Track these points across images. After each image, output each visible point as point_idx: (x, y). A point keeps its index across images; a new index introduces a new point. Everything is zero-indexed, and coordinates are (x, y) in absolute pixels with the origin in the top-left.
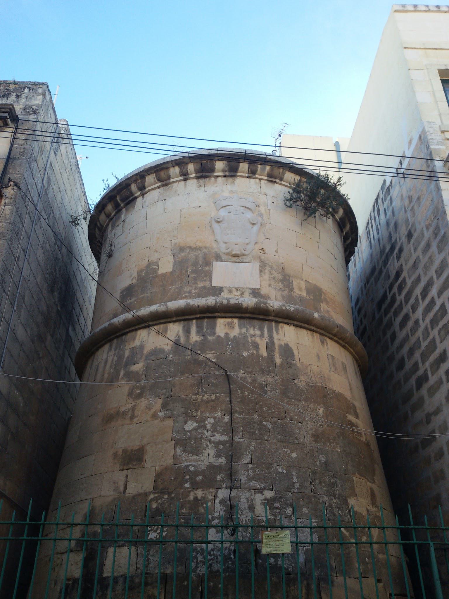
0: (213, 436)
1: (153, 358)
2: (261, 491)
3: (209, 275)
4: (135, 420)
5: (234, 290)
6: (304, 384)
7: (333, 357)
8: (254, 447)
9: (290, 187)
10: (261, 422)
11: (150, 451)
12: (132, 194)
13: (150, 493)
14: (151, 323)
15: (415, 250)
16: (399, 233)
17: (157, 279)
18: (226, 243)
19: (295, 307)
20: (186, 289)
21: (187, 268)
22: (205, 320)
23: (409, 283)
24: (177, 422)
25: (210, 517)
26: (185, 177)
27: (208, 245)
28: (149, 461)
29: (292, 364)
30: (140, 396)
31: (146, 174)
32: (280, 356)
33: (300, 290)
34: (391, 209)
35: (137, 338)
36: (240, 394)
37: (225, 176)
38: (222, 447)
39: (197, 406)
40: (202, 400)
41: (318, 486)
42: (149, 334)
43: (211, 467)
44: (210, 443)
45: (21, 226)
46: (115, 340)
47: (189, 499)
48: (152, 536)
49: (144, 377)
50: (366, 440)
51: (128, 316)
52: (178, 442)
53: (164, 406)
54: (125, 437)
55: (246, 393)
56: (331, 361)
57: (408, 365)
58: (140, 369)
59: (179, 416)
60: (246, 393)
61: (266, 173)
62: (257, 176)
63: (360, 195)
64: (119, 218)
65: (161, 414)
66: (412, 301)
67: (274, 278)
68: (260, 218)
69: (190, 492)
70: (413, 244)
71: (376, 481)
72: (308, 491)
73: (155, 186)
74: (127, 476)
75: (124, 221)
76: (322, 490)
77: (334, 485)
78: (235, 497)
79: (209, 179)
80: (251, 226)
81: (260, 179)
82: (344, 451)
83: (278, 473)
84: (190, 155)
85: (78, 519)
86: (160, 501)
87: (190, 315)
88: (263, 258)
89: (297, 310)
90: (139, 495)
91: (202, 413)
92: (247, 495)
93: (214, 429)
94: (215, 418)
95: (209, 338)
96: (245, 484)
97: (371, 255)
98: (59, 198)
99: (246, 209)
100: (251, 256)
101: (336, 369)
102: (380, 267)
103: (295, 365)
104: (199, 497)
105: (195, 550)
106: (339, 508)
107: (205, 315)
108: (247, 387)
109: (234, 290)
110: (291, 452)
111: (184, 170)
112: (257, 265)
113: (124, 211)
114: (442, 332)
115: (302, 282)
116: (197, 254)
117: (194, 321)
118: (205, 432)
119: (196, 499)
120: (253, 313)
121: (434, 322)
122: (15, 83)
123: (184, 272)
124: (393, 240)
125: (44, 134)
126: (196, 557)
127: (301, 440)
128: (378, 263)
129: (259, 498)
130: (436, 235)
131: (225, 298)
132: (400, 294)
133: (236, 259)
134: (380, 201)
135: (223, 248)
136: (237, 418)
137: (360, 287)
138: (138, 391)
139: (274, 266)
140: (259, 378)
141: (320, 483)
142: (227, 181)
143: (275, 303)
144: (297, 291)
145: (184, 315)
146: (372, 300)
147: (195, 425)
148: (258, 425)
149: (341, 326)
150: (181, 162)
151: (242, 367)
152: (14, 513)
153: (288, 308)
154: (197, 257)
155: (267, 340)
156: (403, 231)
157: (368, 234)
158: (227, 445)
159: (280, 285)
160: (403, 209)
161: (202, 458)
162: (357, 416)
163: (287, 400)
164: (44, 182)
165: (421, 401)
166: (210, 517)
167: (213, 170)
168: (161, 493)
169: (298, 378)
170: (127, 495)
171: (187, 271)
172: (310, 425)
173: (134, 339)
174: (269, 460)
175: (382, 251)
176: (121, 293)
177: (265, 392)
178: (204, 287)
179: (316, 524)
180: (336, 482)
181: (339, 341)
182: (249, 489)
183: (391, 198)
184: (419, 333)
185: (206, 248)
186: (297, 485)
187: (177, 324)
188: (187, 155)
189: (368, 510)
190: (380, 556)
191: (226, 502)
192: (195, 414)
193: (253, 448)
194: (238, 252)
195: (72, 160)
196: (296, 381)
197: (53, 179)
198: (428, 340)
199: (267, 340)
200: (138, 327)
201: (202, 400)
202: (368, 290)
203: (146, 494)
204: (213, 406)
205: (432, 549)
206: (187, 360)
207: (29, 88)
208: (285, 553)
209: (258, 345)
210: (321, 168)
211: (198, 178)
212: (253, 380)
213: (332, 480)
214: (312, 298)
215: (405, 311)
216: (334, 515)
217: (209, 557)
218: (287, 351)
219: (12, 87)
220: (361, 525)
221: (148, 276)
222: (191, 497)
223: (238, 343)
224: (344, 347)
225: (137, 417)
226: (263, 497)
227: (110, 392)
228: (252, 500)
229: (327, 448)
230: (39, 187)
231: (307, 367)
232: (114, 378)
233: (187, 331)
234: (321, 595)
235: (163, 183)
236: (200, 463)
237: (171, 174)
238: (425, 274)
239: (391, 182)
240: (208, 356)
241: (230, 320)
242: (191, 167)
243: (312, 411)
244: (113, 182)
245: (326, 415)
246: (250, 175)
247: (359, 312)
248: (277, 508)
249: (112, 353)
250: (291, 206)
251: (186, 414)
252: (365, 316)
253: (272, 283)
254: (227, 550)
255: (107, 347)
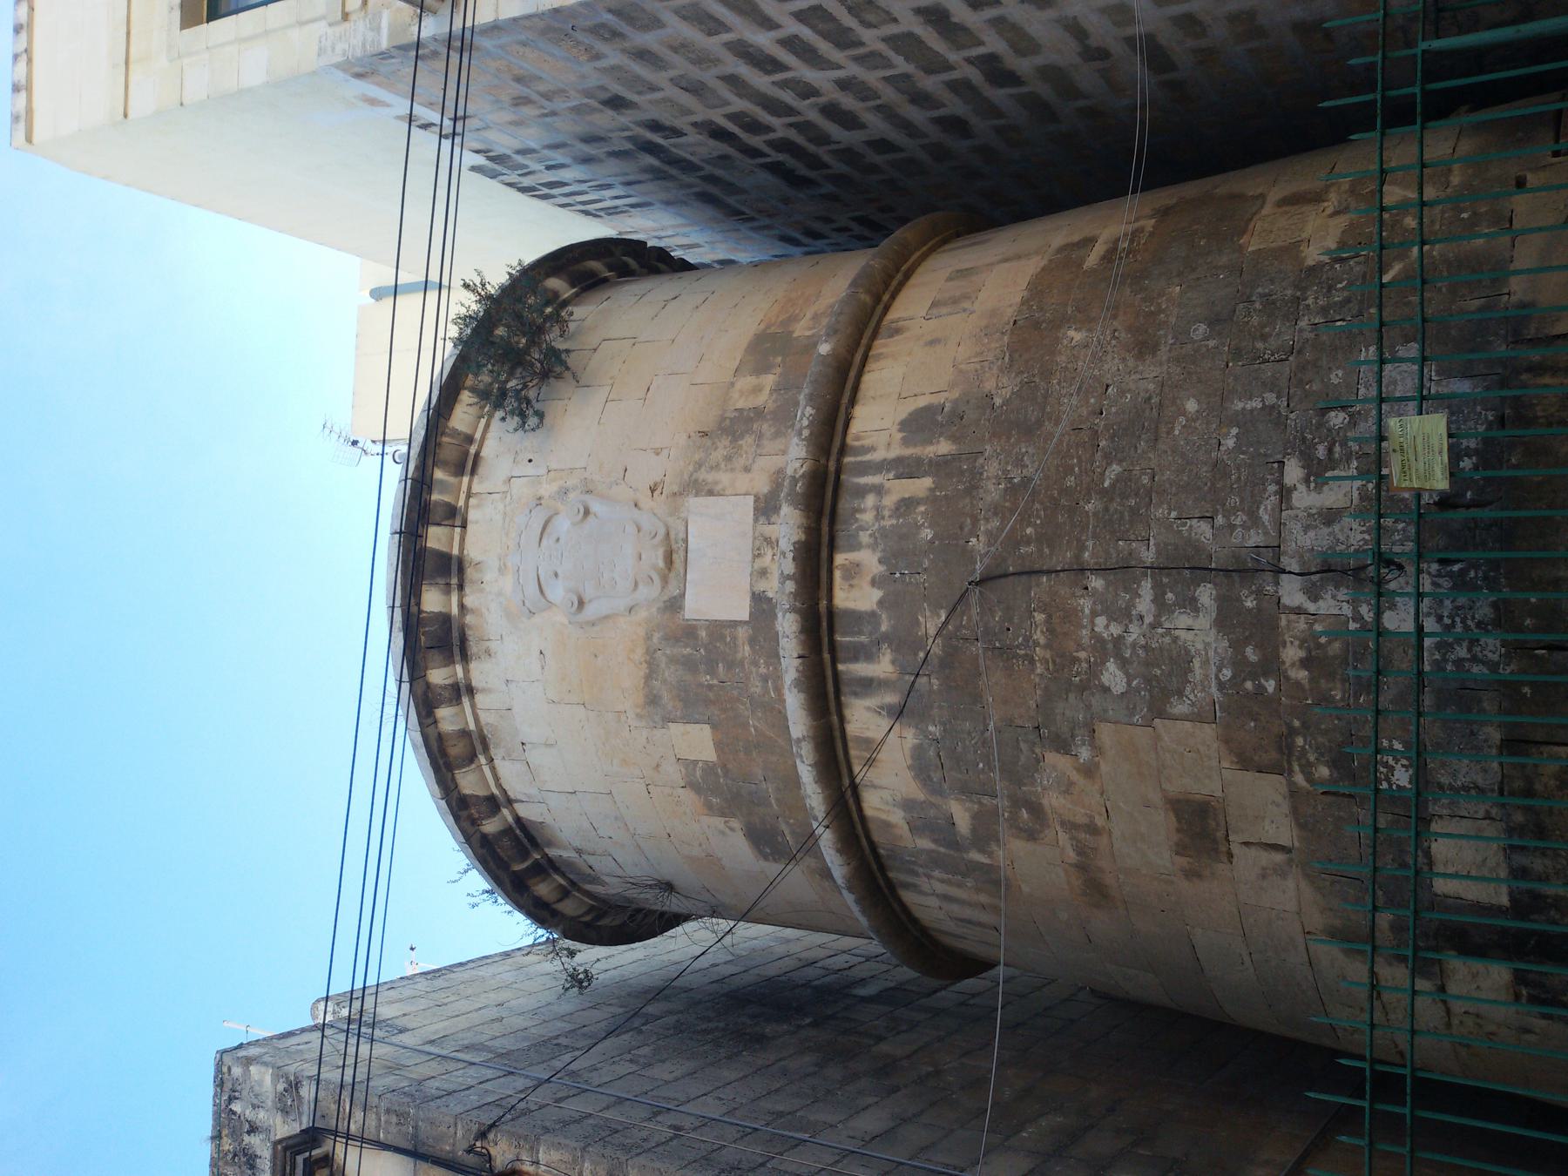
0: (1142, 617)
1: (936, 776)
2: (1285, 493)
3: (720, 629)
4: (1100, 821)
5: (759, 564)
6: (1005, 380)
7: (934, 305)
8: (1170, 510)
9: (491, 416)
10: (1104, 493)
11: (1179, 785)
12: (507, 831)
13: (1291, 784)
14: (846, 782)
15: (653, 88)
16: (611, 131)
17: (730, 766)
18: (636, 584)
19: (802, 402)
20: (758, 690)
21: (701, 685)
22: (838, 638)
23: (739, 104)
24: (1105, 711)
25: (1353, 626)
26: (461, 691)
27: (641, 632)
28: (1208, 787)
29: (953, 412)
30: (1037, 810)
31: (455, 794)
32: (932, 443)
33: (760, 390)
34: (546, 152)
35: (884, 816)
36: (1032, 548)
37: (461, 587)
38: (1170, 595)
39: (1063, 660)
40: (1047, 646)
41: (1273, 343)
42: (875, 787)
43: (1221, 623)
44: (1160, 625)
45: (591, 1121)
46: (891, 875)
47: (1305, 682)
48: (1402, 777)
49: (986, 800)
50: (1152, 217)
51: (827, 841)
52: (1159, 711)
53: (1063, 745)
54: (1144, 849)
55: (1029, 531)
56: (944, 310)
57: (955, 106)
58: (967, 810)
59: (1089, 707)
60: (1029, 531)
61: (452, 480)
62: (461, 503)
63: (509, 233)
64: (570, 864)
65: (1085, 754)
66: (788, 97)
67: (728, 459)
68: (572, 496)
69: (1287, 678)
70: (639, 93)
71: (1259, 191)
72: (1286, 369)
73: (486, 770)
74: (1246, 844)
75: (579, 851)
76: (1282, 334)
77: (1269, 302)
78: (1302, 562)
79: (470, 628)
80: (591, 518)
81: (469, 495)
82: (1180, 274)
83: (1238, 448)
84: (406, 677)
85: (1358, 971)
86: (1312, 758)
87: (824, 677)
88: (675, 488)
89: (811, 399)
90: (1295, 811)
91: (1080, 647)
92: (1295, 528)
93: (1125, 615)
94: (1094, 614)
95: (884, 628)
96: (1266, 533)
97: (668, 203)
98: (520, 1022)
99: (548, 530)
100: (670, 520)
101: (966, 297)
102: (698, 181)
103: (956, 402)
104: (1302, 654)
105: (1439, 666)
106: (1329, 290)
107: (826, 640)
108: (1013, 529)
109: (759, 564)
110: (1184, 413)
111: (446, 694)
112: (694, 503)
113: (553, 852)
114: (870, 17)
115: (738, 386)
116: (664, 659)
117: (841, 667)
118: (1130, 639)
119: (1305, 663)
120: (819, 514)
121: (843, 39)
122: (217, 1137)
123: (711, 695)
124: (628, 146)
125: (350, 1061)
126: (1459, 663)
127: (1151, 386)
128: (690, 186)
129: (1304, 499)
130: (616, 35)
131: (780, 584)
132: (769, 129)
133: (678, 559)
134: (527, 182)
135: (650, 592)
136: (1093, 555)
137: (751, 234)
138: (1024, 814)
139: (697, 457)
140: (989, 499)
141: (1264, 338)
142: (472, 582)
143: (794, 456)
144: (762, 399)
145: (826, 693)
146: (786, 201)
147: (1111, 666)
148: (1112, 500)
149: (854, 284)
150: (425, 702)
151: (962, 542)
152: (1343, 1138)
153: (805, 422)
154: (673, 660)
155: (891, 476)
156: (606, 120)
157: (612, 212)
158: (1165, 580)
159: (748, 441)
160: (548, 119)
161: (1200, 646)
162: (1090, 242)
163: (1048, 426)
164: (476, 1060)
165: (1050, 73)
166: (1353, 626)
167: (445, 619)
168: (1290, 755)
169: (990, 396)
170: (1297, 844)
171: (710, 687)
172: (1112, 365)
173: (887, 825)
174: (1204, 471)
175: (658, 175)
176: (766, 858)
177: (1026, 481)
178: (752, 641)
179: (1372, 349)
180: (1261, 296)
181: (892, 288)
182: (1280, 525)
183: (518, 152)
184: (872, 78)
185: (649, 637)
186: (1271, 398)
187: (847, 713)
188: (406, 687)
189: (1336, 213)
190: (1456, 180)
191: (1314, 584)
192: (1085, 665)
193: (1174, 514)
194: (660, 552)
195: (418, 986)
196: (998, 401)
197: (469, 1038)
198: (891, 54)
199: (891, 476)
200: (855, 816)
201: (1047, 646)
202: (760, 212)
203: (1294, 793)
204: (1062, 619)
205: (1437, 44)
206: (944, 685)
207: (231, 1100)
208: (1449, 428)
209: (903, 500)
210: (441, 334)
211: (465, 658)
212: (996, 514)
213: (1258, 306)
214: (779, 359)
215: (814, 116)
216: (1348, 300)
217: (1459, 628)
218: (919, 424)
219: (227, 1145)
220: (1376, 229)
221: (721, 788)
222: (1302, 675)
223: (898, 552)
224: (908, 276)
225: (1092, 817)
226: (1302, 488)
227: (1026, 889)
228: (1310, 515)
229: (1173, 320)
230: (490, 1073)
231: (961, 371)
232: (990, 878)
233: (868, 686)
234: (1558, 337)
235: (479, 748)
236: (1211, 653)
237: (456, 728)
238: (716, 61)
239: (477, 152)
240: (932, 631)
241: (837, 574)
242: (438, 676)
243: (1076, 358)
244: (478, 881)
245: (1087, 322)
246: (458, 523)
247: (816, 235)
248: (1330, 450)
249: (923, 882)
250: (540, 415)
251: (1083, 688)
252: (827, 220)
253: (740, 462)
254: (1440, 581)
255: (908, 897)
